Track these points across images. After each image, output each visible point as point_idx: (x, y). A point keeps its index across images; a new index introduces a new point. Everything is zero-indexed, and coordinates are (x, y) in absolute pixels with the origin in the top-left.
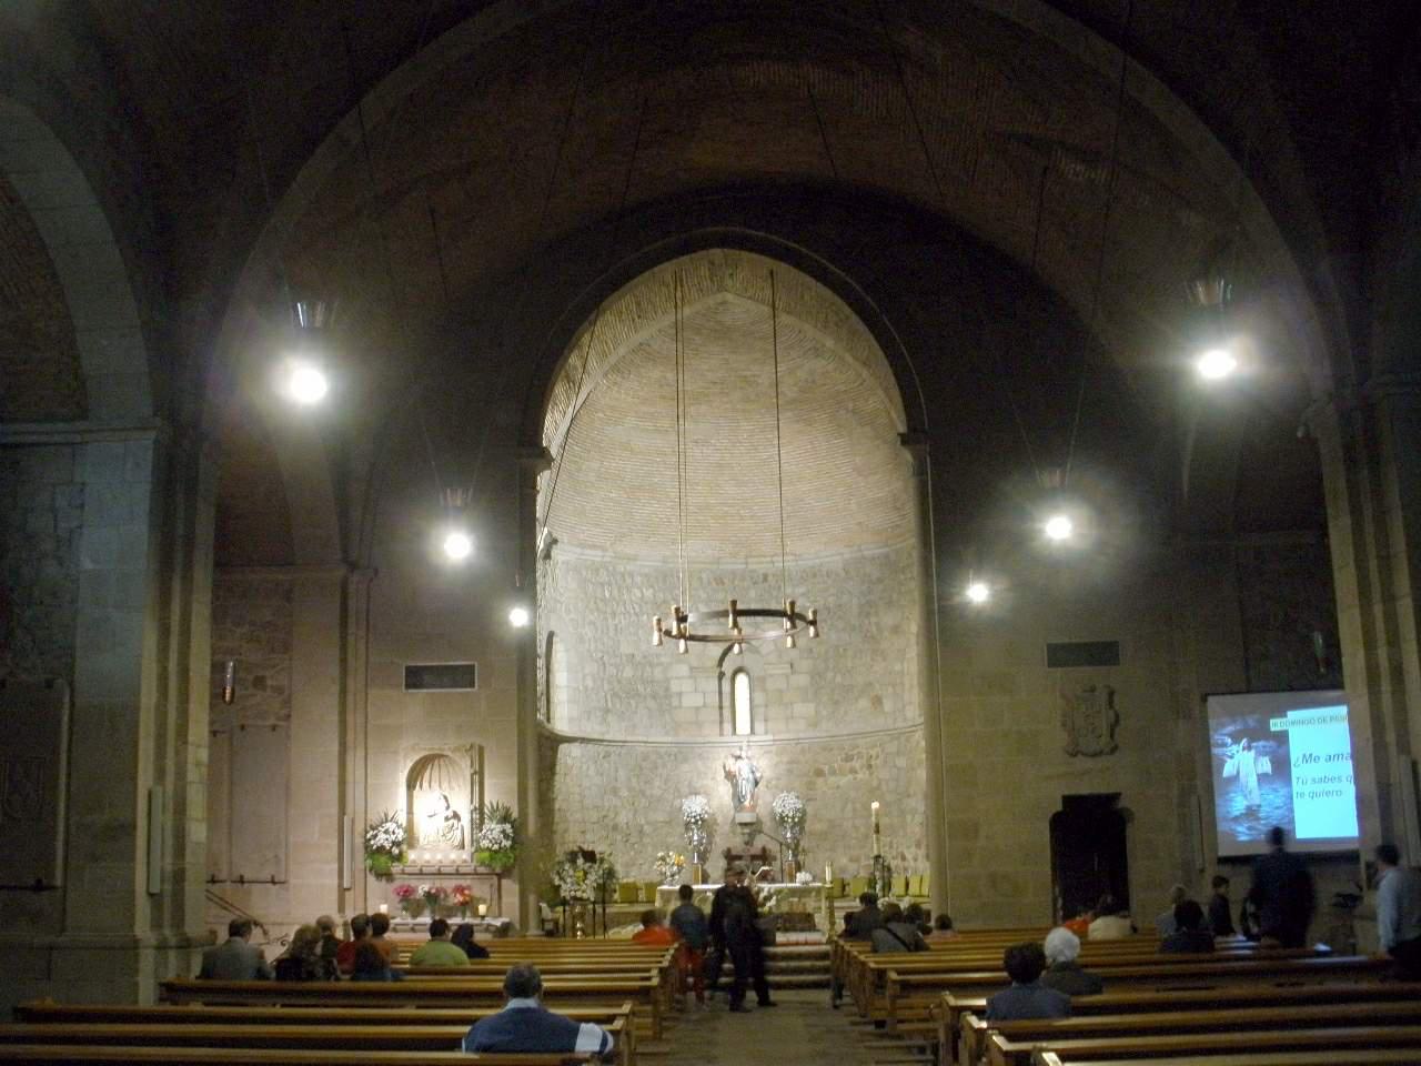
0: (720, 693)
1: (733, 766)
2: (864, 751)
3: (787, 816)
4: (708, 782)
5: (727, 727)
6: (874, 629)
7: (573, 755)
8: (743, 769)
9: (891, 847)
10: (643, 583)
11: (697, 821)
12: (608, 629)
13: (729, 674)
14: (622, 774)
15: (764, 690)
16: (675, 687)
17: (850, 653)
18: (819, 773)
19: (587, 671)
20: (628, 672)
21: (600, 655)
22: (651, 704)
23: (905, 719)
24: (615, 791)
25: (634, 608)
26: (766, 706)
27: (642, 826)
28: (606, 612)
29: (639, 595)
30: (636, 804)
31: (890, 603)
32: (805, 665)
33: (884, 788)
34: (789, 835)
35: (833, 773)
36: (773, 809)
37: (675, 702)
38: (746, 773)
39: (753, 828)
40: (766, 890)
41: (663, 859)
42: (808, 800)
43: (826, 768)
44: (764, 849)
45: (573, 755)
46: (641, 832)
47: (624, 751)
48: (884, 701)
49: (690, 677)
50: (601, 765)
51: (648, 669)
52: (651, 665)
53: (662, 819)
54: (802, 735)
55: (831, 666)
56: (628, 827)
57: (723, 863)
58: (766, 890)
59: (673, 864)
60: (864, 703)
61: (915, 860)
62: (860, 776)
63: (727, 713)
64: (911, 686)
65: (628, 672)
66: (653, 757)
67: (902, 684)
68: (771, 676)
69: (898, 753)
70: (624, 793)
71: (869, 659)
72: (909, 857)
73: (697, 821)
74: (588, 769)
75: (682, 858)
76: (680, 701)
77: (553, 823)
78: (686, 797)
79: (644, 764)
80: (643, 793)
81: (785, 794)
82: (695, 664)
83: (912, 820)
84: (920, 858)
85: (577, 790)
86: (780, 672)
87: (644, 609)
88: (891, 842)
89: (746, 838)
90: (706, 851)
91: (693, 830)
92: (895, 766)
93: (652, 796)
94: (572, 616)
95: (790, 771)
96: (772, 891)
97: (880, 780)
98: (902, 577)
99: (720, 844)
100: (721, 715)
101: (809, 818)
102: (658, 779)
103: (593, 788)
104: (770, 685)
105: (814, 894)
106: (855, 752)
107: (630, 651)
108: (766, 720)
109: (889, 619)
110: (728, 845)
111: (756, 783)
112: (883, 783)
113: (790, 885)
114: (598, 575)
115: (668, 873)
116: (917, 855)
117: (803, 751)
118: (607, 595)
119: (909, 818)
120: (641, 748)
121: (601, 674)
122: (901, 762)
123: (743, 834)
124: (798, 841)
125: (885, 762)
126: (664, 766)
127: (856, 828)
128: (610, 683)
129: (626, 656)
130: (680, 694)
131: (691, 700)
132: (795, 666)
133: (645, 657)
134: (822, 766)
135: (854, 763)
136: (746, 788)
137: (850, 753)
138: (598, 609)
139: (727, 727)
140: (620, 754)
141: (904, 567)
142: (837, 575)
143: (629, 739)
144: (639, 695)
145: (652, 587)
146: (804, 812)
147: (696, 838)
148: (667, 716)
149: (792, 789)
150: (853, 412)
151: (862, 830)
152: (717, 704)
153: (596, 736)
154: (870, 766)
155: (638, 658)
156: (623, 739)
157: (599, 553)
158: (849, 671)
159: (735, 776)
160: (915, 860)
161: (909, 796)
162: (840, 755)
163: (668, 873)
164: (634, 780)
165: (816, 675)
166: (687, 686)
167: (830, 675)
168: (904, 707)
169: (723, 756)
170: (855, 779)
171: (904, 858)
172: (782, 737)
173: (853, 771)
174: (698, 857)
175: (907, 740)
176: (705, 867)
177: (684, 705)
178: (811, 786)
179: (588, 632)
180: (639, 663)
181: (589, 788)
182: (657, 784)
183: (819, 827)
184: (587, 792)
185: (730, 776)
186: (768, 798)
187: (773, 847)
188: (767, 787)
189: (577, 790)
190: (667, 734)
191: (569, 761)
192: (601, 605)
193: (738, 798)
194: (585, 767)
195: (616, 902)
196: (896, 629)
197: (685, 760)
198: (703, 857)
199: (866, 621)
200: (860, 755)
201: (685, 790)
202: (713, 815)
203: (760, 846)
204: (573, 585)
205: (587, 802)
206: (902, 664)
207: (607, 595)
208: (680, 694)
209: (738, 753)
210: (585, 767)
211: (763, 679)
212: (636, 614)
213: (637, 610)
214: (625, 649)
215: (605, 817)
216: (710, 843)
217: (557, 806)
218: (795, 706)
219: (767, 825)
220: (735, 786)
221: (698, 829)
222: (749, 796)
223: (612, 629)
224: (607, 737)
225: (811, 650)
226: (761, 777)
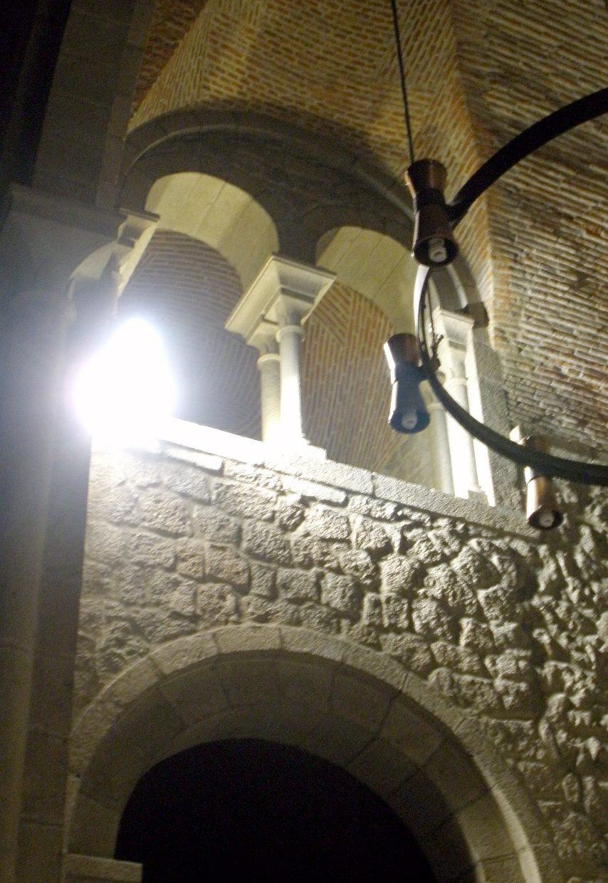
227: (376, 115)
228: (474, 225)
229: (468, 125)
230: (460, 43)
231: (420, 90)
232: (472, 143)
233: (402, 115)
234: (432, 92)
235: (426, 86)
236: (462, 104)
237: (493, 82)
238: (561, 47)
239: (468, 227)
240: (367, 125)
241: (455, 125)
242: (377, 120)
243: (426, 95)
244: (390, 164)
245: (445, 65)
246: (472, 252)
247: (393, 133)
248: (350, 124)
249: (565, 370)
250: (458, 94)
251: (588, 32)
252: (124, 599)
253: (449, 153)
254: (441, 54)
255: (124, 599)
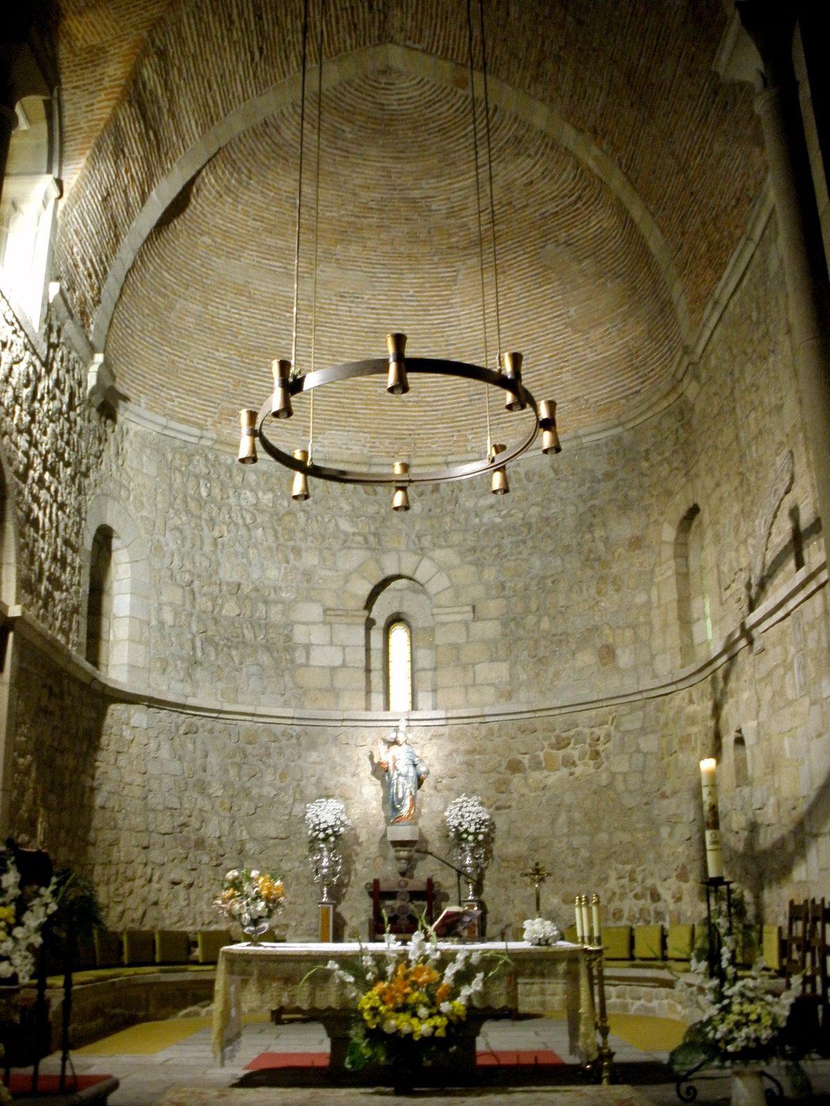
0: (368, 649)
1: (384, 755)
2: (587, 731)
3: (466, 831)
4: (346, 779)
5: (377, 699)
6: (601, 546)
7: (133, 722)
8: (398, 759)
9: (632, 880)
10: (258, 484)
11: (328, 836)
12: (202, 543)
13: (381, 623)
14: (213, 760)
15: (434, 647)
16: (300, 635)
17: (562, 586)
18: (515, 767)
19: (164, 599)
20: (230, 609)
21: (187, 577)
22: (265, 658)
23: (655, 676)
24: (202, 787)
25: (243, 518)
26: (435, 669)
27: (243, 842)
28: (200, 517)
29: (252, 500)
30: (235, 808)
31: (626, 506)
32: (494, 607)
33: (620, 785)
34: (468, 861)
35: (537, 766)
36: (444, 821)
37: (300, 656)
38: (403, 766)
39: (413, 849)
40: (460, 957)
41: (236, 884)
42: (498, 808)
43: (526, 760)
44: (430, 883)
45: (133, 722)
46: (241, 852)
47: (219, 726)
48: (619, 652)
49: (324, 623)
50: (183, 746)
51: (261, 606)
52: (266, 602)
53: (274, 834)
54: (487, 711)
55: (534, 606)
56: (221, 844)
57: (366, 903)
58: (460, 957)
59: (258, 896)
60: (586, 658)
61: (678, 899)
62: (578, 770)
63: (376, 678)
64: (665, 625)
65: (230, 609)
66: (264, 739)
67: (649, 623)
68: (443, 624)
69: (643, 731)
70: (216, 790)
71: (593, 591)
72: (666, 895)
73: (328, 836)
74: (158, 749)
75: (278, 883)
76: (308, 658)
77: (87, 829)
78: (312, 801)
79: (249, 748)
80: (247, 793)
81: (463, 798)
82: (331, 603)
83: (671, 835)
84: (686, 898)
85: (138, 780)
86: (458, 617)
87: (259, 520)
88: (632, 872)
89: (403, 865)
90: (341, 884)
91: (321, 850)
92: (638, 751)
93: (261, 796)
94: (145, 513)
95: (470, 765)
96: (475, 959)
97: (613, 775)
98: (645, 464)
99: (363, 873)
100: (368, 681)
101: (499, 834)
102: (271, 771)
103: (167, 780)
104: (441, 638)
105: (562, 967)
106: (572, 733)
107: (236, 578)
108: (434, 691)
109: (623, 529)
110: (376, 877)
111: (420, 782)
112: (620, 778)
113: (513, 945)
114: (190, 462)
115: (246, 916)
116: (681, 892)
117: (491, 732)
118: (204, 493)
119: (665, 831)
120: (245, 724)
121: (188, 607)
122: (649, 743)
123: (398, 859)
124: (483, 870)
125: (623, 745)
126: (281, 752)
127: (575, 851)
128: (199, 619)
129: (228, 584)
130: (308, 647)
131: (324, 657)
132: (478, 607)
133: (256, 590)
134: (520, 757)
135: (568, 750)
136: (404, 787)
137: (564, 735)
138: (188, 512)
139: (377, 699)
140: (211, 731)
141: (647, 451)
142: (542, 476)
143: (227, 707)
144: (245, 644)
145: (271, 490)
146: (492, 826)
147: (325, 862)
148: (287, 678)
149: (474, 792)
150: (567, 244)
151: (584, 853)
152: (363, 664)
153: (171, 698)
154: (596, 754)
155: (246, 589)
156: (218, 707)
157: (196, 431)
158: (561, 612)
159: (387, 771)
160: (678, 899)
161: (663, 796)
162: (545, 739)
163: (246, 916)
164: (233, 772)
165: (510, 621)
166: (318, 635)
167: (531, 620)
168: (653, 657)
169: (369, 740)
170: (571, 774)
171: (656, 897)
172: (455, 713)
173: (569, 763)
174: (328, 893)
175: (659, 709)
176: (339, 909)
177: (312, 662)
178: (502, 786)
179: (171, 542)
180: (247, 597)
181: (160, 778)
182: (269, 778)
183: (513, 849)
184: (154, 785)
185: (381, 771)
186: (437, 804)
187: (446, 880)
188: (435, 788)
189: (138, 780)
190: (286, 704)
191: (127, 734)
192: (193, 505)
193: (391, 804)
194: (153, 745)
195: (196, 963)
196: (636, 543)
197: (313, 746)
198: (336, 894)
199: (588, 536)
200: (579, 738)
201: (311, 790)
202: (352, 829)
203: (425, 879)
204: (151, 469)
205: (153, 800)
206: (648, 592)
207: (204, 493)
208: (308, 647)
209: (391, 736)
210: (153, 745)
211: (431, 631)
212: (246, 526)
213: (248, 521)
214: (228, 573)
215: (184, 825)
216: (348, 872)
217: (99, 800)
218: (478, 668)
219: (435, 845)
220: (387, 785)
221: (330, 850)
222: (407, 802)
223: (208, 542)
224: (191, 701)
225: (503, 586)
226: (427, 773)
227: (80, 13)
228: (87, 129)
229: (128, 69)
230: (162, 18)
231: (118, 23)
232: (123, 82)
233: (610, 978)
234: (122, 30)
235: (122, 24)
236: (134, 53)
237: (156, 53)
238: (193, 56)
239: (78, 126)
240: (70, 13)
241: (120, 62)
242: (78, 16)
243: (118, 29)
244: (62, 47)
245: (142, 23)
246: (72, 143)
247: (79, 32)
248: (62, 5)
249: (75, 250)
250: (137, 46)
251: (208, 56)
252: (204, 1096)
253: (102, 74)
254: (146, 15)
255: (204, 1096)
